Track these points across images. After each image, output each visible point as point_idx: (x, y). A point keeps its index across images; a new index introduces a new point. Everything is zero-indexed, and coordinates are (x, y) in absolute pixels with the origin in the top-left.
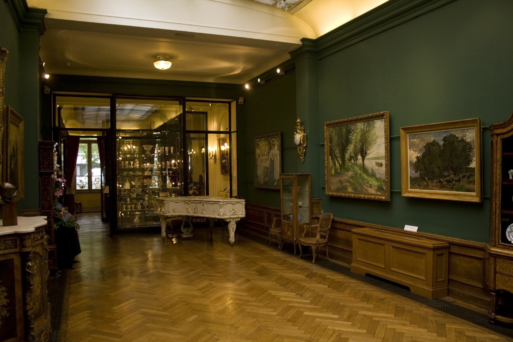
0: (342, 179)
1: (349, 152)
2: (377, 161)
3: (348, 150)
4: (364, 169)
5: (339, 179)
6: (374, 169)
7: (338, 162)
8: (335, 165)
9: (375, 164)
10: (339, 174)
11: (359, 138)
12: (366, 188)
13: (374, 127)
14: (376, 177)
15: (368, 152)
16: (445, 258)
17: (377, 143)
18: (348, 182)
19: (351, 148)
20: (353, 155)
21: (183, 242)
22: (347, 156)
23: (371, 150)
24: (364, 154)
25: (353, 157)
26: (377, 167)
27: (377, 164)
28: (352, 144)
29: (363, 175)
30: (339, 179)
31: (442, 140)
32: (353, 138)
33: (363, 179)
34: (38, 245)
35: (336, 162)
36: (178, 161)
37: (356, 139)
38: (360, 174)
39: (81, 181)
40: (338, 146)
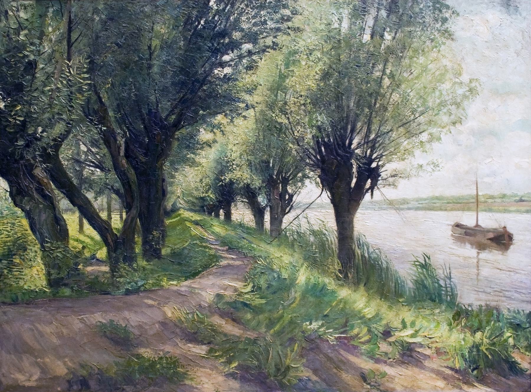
0: (132, 319)
1: (207, 159)
2: (468, 219)
3: (192, 144)
4: (353, 262)
6: (438, 260)
8: (61, 232)
10: (97, 289)
11: (306, 78)
12: (366, 365)
13: (448, 34)
14: (452, 303)
15: (387, 169)
17: (470, 124)
18: (193, 337)
19: (224, 143)
20: (243, 175)
22: (187, 180)
23: (419, 157)
24: (348, 177)
25: (250, 194)
26: (469, 251)
27: (465, 234)
28: (235, 113)
29: (344, 293)
30: (98, 318)
33: (346, 318)
34: (85, 236)
35: (72, 219)
36: (50, 29)
38: (317, 292)
39: (235, 36)
40: (95, 113)
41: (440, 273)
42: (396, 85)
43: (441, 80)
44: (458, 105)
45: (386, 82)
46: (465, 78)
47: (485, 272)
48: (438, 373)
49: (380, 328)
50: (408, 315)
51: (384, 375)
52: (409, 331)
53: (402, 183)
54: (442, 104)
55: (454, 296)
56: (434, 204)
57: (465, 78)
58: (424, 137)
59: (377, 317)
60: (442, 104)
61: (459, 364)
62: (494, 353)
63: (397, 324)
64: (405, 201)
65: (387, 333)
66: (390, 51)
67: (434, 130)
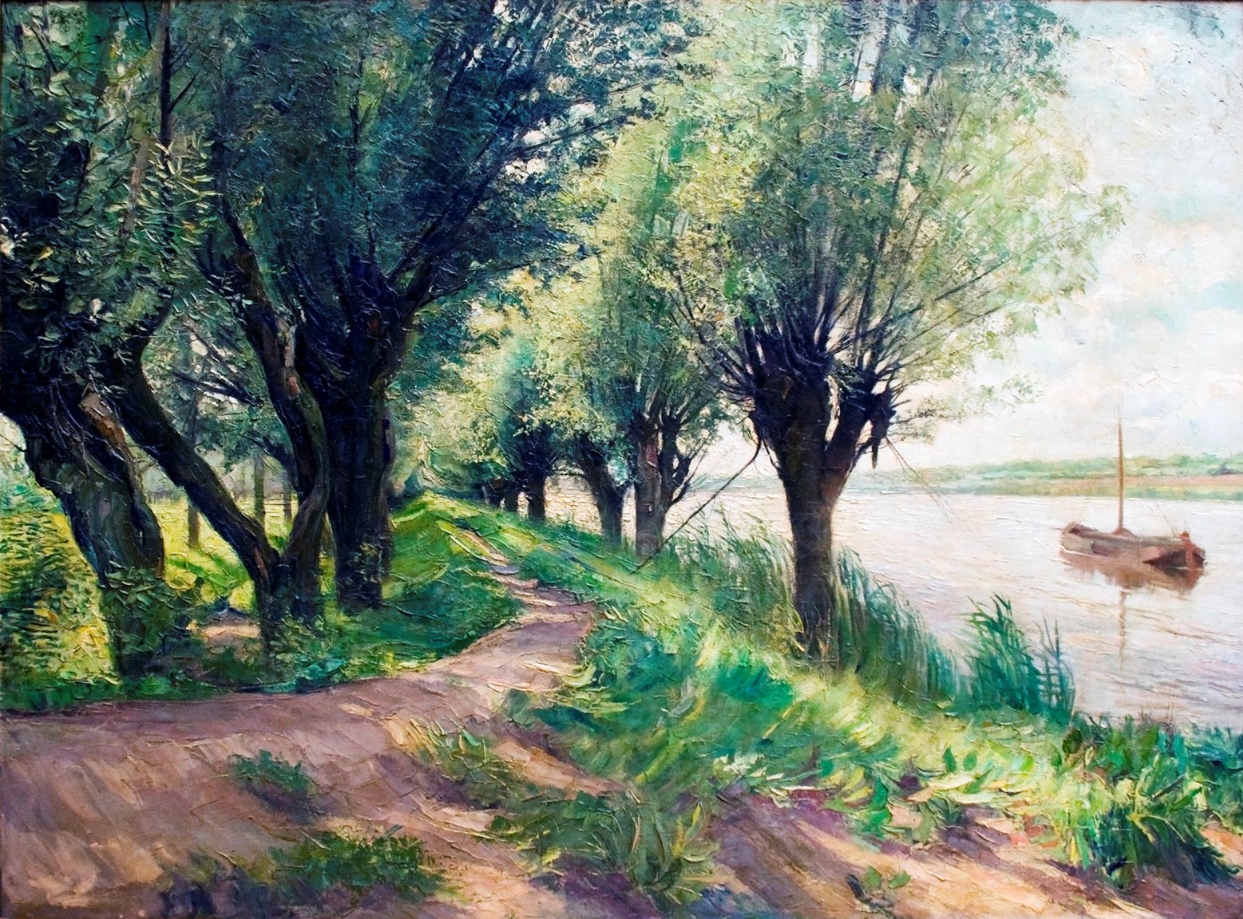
1: (488, 373)
2: (1100, 516)
4: (834, 619)
5: (234, 746)
6: (1029, 614)
7: (209, 501)
9: (1053, 544)
11: (719, 185)
13: (1051, 81)
14: (1061, 713)
16: (1113, 471)
17: (1103, 293)
18: (456, 792)
19: (529, 336)
21: (425, 696)
22: (441, 425)
23: (984, 371)
24: (818, 414)
27: (1094, 549)
29: (809, 687)
30: (234, 746)
31: (328, 691)
32: (582, 186)
33: (813, 749)
35: (172, 514)
37: (655, 203)
40: (225, 266)
41: (1034, 642)
42: (931, 200)
43: (1035, 188)
44: (1076, 248)
45: (908, 193)
46: (1093, 184)
47: (1140, 639)
48: (1029, 876)
49: (890, 770)
50: (957, 737)
51: (902, 880)
52: (962, 778)
53: (944, 430)
54: (1039, 246)
55: (1065, 695)
56: (1018, 480)
57: (1093, 184)
58: (997, 322)
59: (887, 747)
60: (1039, 246)
61: (1077, 855)
62: (1160, 829)
63: (932, 760)
64: (951, 474)
65: (910, 784)
66: (917, 120)
67: (1020, 307)
